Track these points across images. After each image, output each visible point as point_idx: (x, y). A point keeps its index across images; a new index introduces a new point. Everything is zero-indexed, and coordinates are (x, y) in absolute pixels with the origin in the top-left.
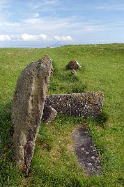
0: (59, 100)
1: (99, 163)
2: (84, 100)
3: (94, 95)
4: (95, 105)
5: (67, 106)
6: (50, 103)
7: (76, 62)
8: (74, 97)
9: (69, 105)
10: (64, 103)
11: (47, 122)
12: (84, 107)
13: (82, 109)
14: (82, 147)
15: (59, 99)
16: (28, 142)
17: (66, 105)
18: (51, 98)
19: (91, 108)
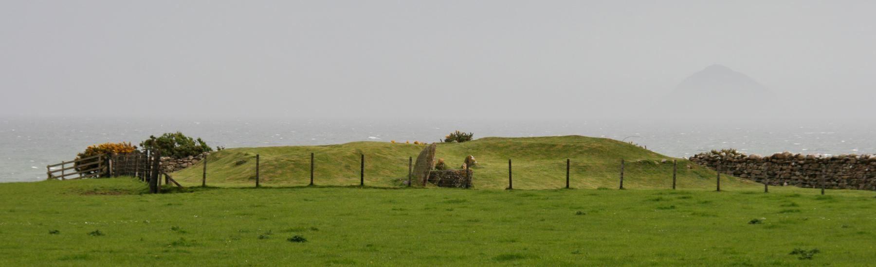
7: (471, 157)
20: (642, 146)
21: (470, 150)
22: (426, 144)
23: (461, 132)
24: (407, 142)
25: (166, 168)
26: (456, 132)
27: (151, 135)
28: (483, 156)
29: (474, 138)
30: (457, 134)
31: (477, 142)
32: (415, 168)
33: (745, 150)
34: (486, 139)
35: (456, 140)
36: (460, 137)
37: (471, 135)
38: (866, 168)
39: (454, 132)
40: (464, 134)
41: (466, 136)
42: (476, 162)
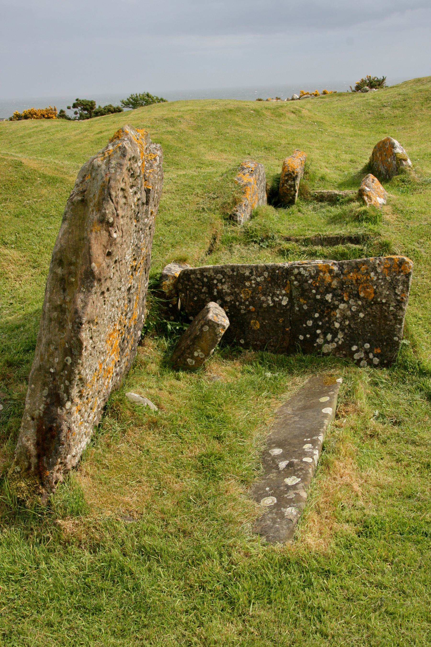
0: (248, 284)
1: (278, 506)
2: (335, 283)
3: (374, 269)
4: (376, 303)
5: (274, 306)
6: (218, 292)
7: (393, 146)
8: (299, 273)
9: (284, 303)
10: (264, 295)
11: (193, 357)
12: (338, 311)
13: (330, 319)
14: (279, 445)
15: (248, 279)
16: (47, 411)
17: (273, 301)
18: (220, 276)
19: (361, 315)
20: (96, 103)
21: (385, 109)
22: (335, 92)
23: (373, 76)
24: (77, 100)
25: (21, 298)
26: (367, 77)
27: (76, 99)
28: (418, 124)
29: (387, 83)
30: (368, 79)
31: (401, 91)
32: (161, 298)
33: (36, 108)
34: (419, 81)
35: (367, 86)
36: (372, 83)
37: (384, 80)
38: (188, 310)
39: (364, 78)
40: (376, 79)
41: (378, 81)
42: (409, 162)
